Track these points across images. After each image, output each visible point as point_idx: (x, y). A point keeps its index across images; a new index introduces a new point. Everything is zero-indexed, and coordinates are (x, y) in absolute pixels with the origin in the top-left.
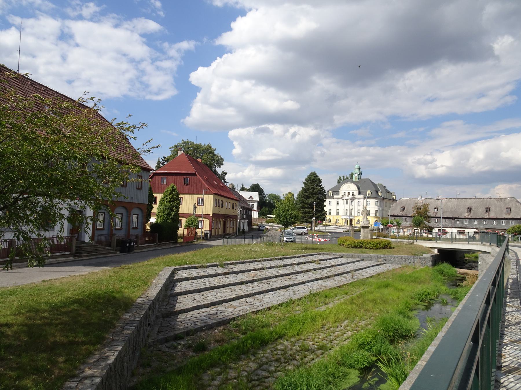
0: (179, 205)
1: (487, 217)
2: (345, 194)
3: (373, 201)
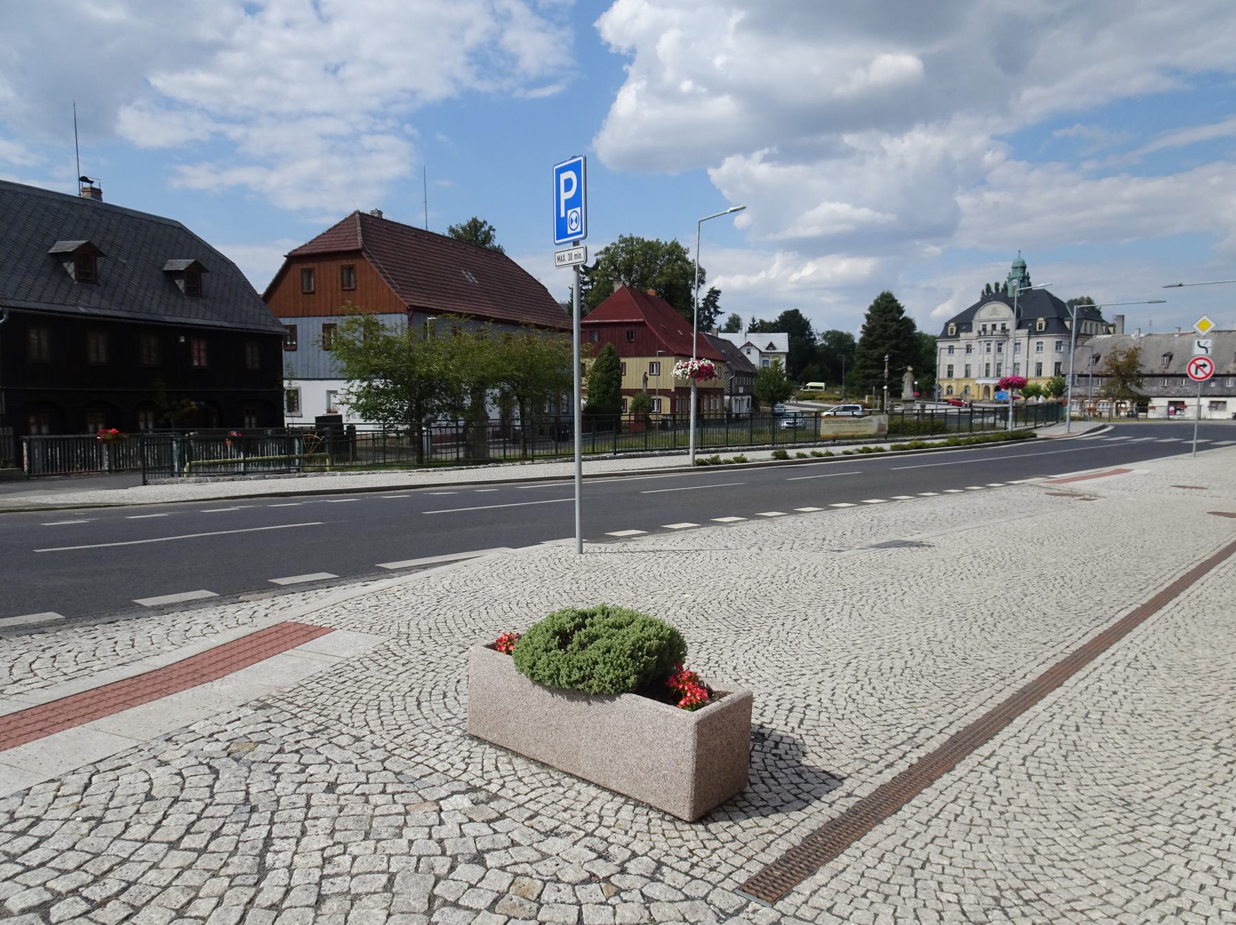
0: (620, 376)
2: (984, 329)
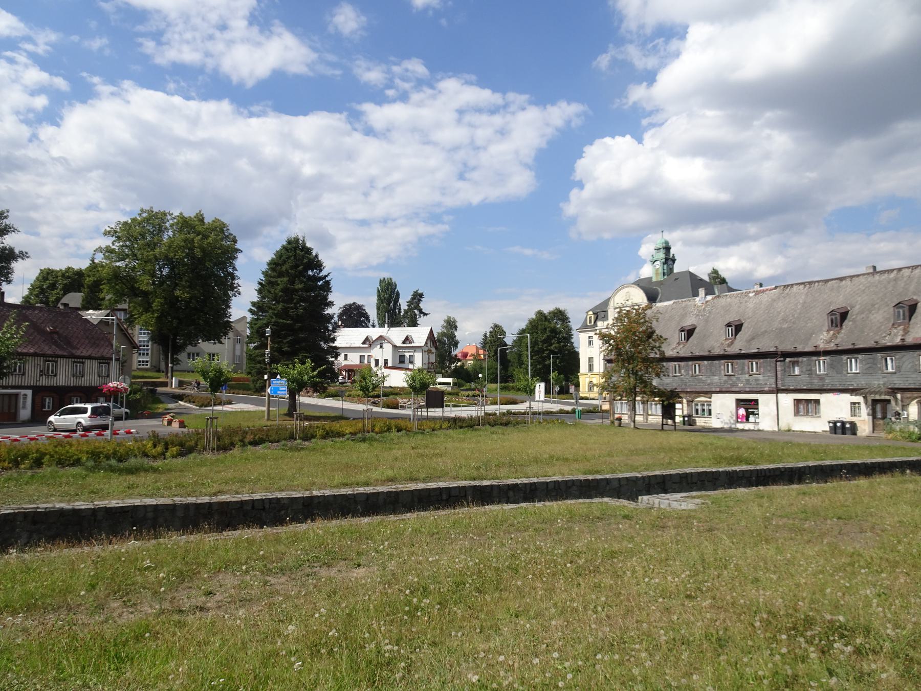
1: (897, 341)
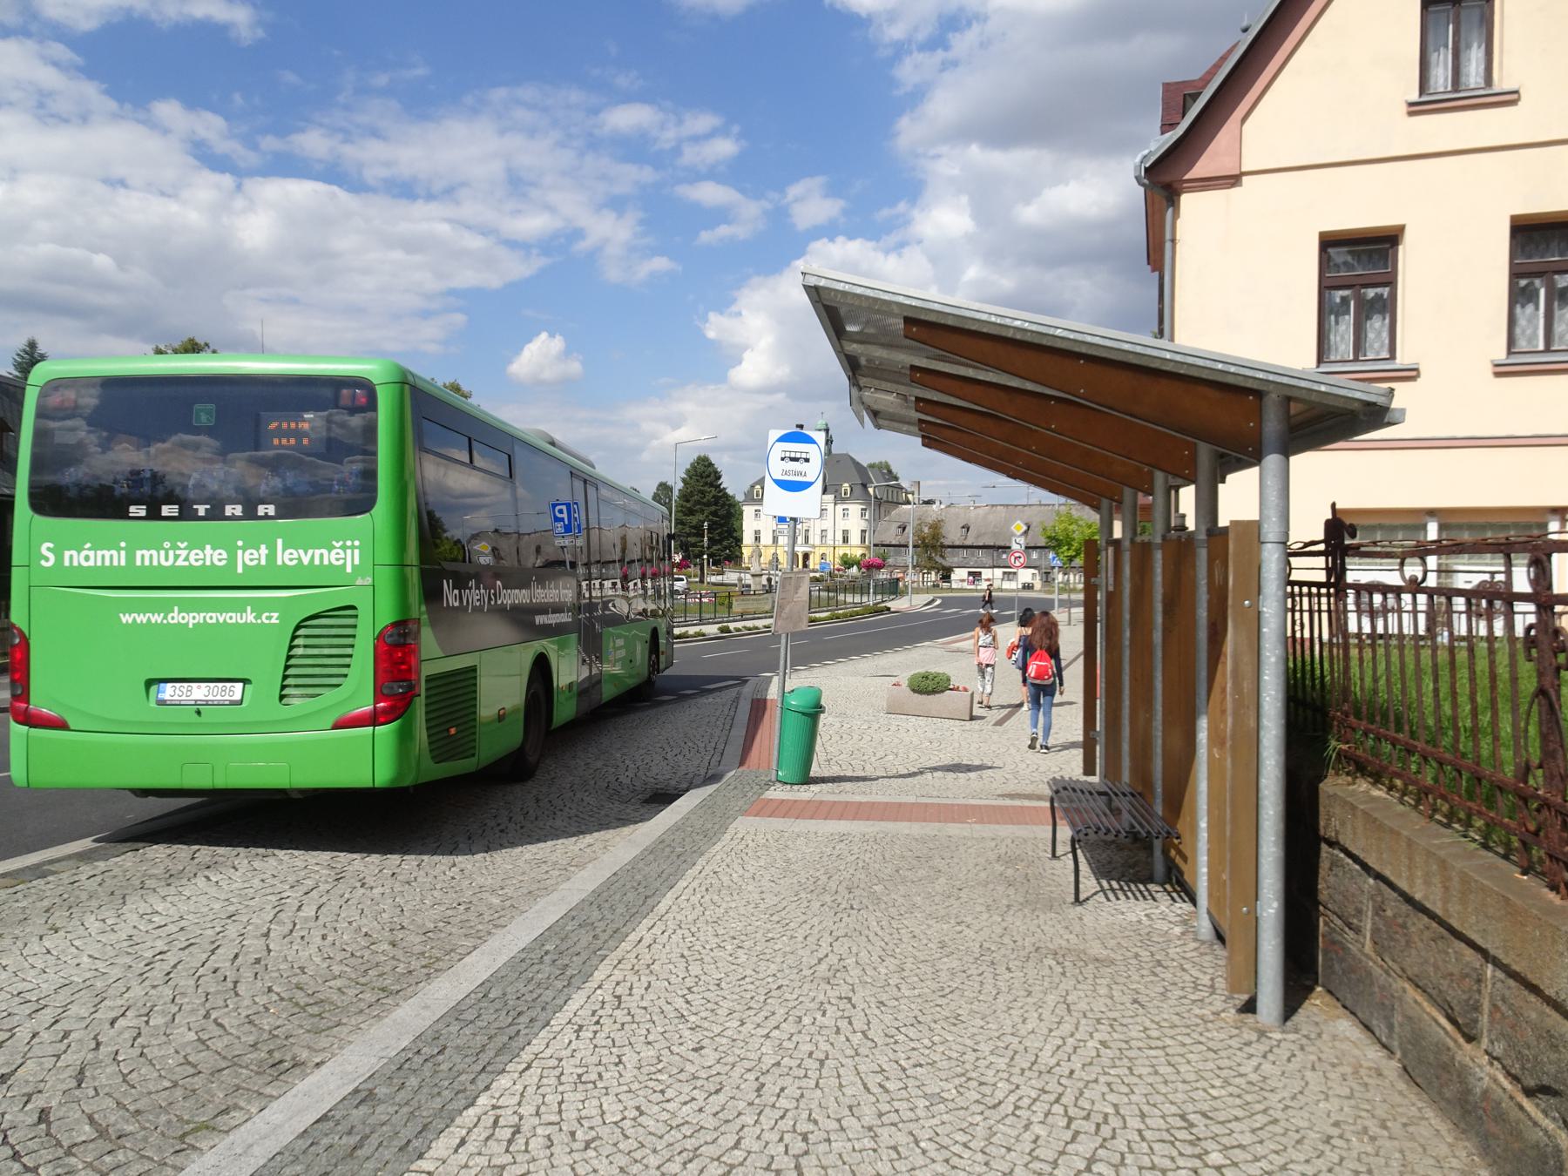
3: (855, 509)
